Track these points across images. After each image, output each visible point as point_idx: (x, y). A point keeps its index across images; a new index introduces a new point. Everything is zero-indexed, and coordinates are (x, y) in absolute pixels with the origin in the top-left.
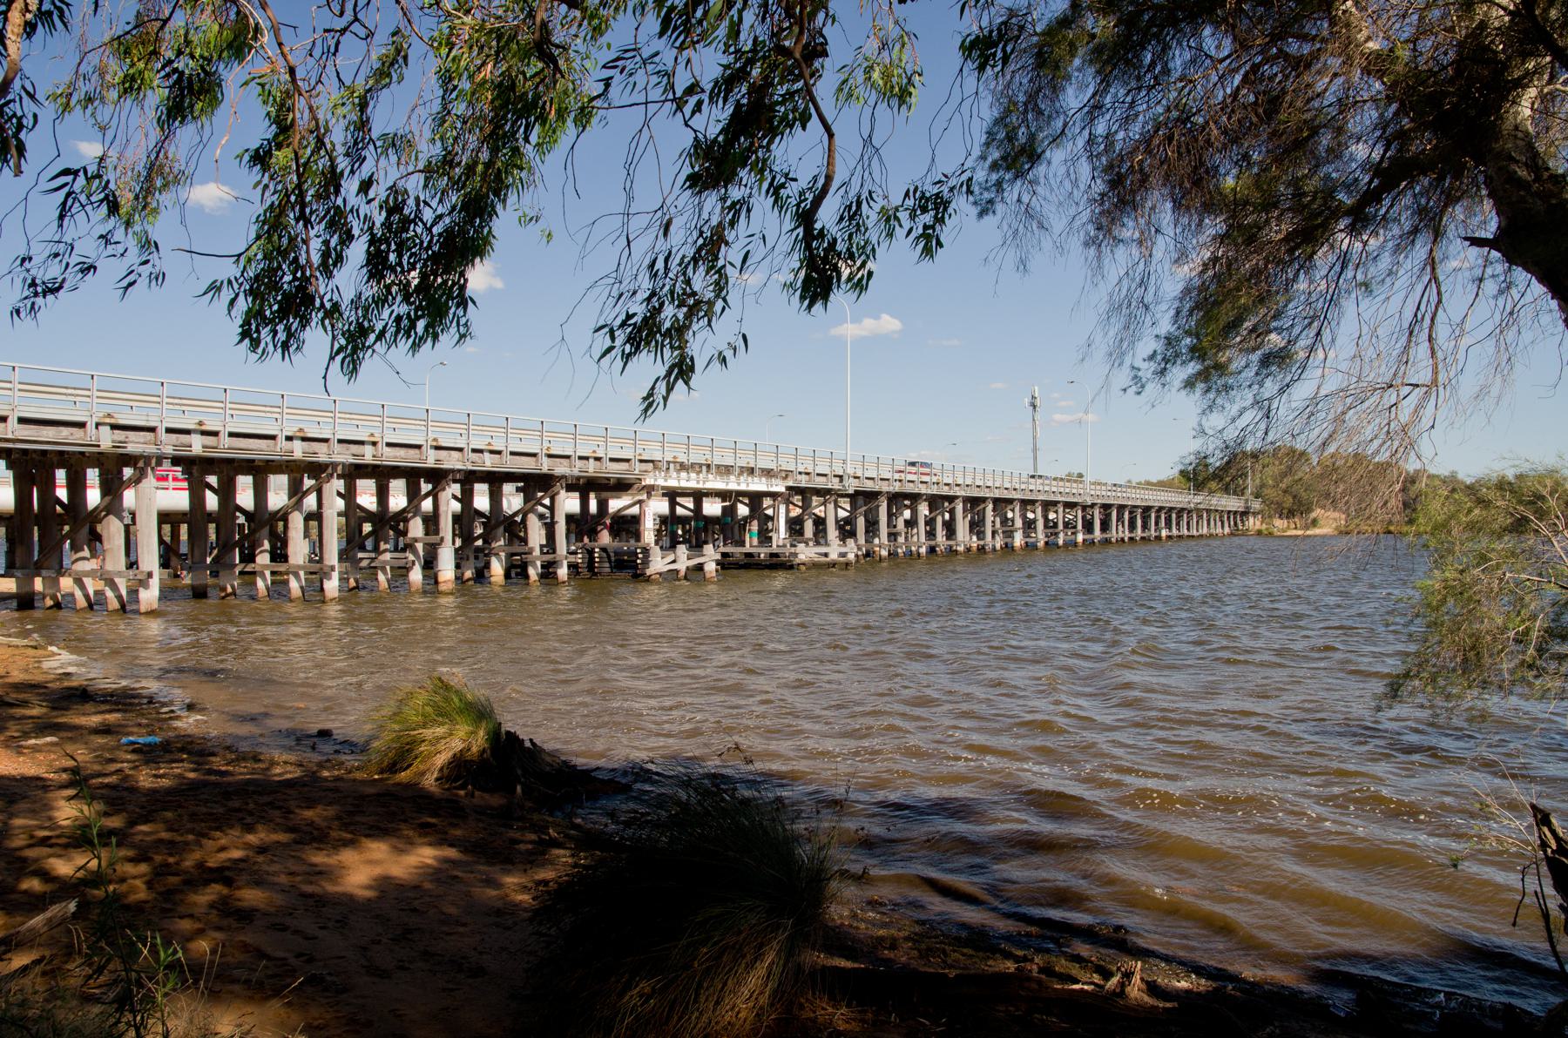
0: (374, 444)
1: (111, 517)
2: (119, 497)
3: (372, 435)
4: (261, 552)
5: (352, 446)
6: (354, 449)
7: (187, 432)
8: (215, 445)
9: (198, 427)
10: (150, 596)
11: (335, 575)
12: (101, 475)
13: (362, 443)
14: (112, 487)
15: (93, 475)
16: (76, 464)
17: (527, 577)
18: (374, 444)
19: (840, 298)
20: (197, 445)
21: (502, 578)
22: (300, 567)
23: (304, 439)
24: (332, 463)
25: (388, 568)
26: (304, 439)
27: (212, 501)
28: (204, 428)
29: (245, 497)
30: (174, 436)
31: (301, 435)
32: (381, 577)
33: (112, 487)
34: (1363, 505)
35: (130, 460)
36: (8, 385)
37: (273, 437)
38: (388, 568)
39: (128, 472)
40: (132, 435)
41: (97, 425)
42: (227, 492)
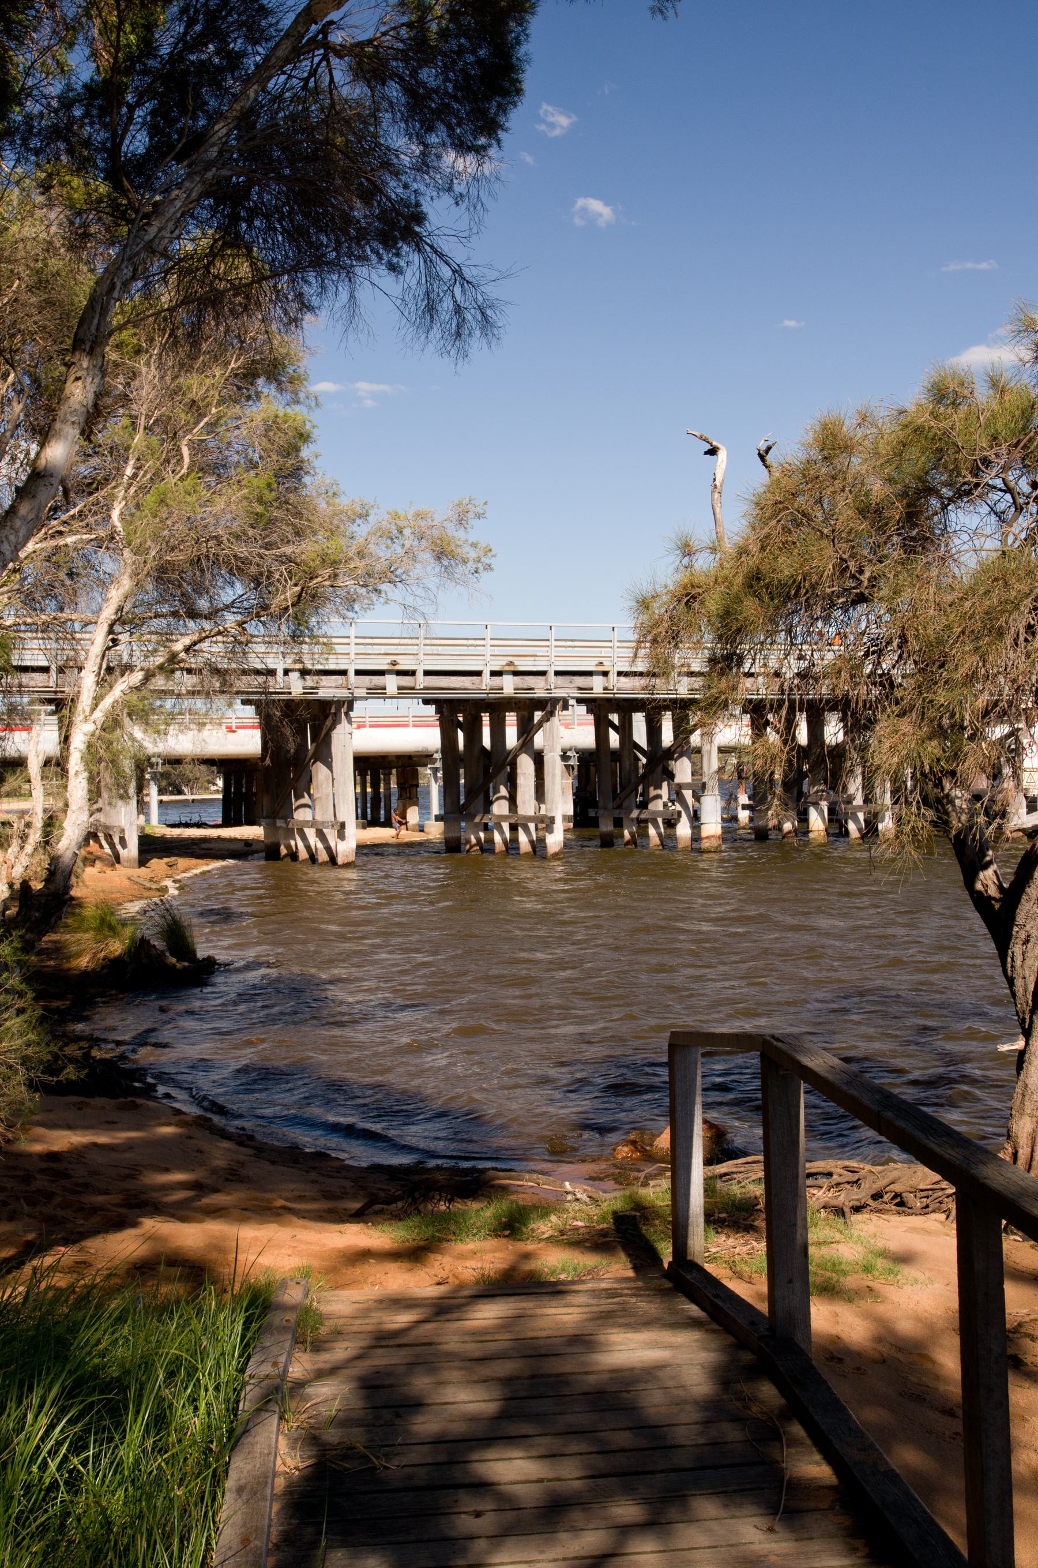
0: (605, 674)
1: (319, 764)
2: (687, 740)
3: (601, 664)
4: (498, 799)
5: (576, 678)
6: (580, 681)
7: (381, 673)
8: (411, 685)
9: (391, 667)
10: (555, 840)
11: (888, 815)
12: (646, 717)
13: (589, 674)
14: (526, 730)
15: (511, 719)
16: (497, 707)
17: (847, 833)
18: (605, 674)
19: (476, 344)
20: (597, 686)
21: (823, 833)
22: (530, 819)
23: (516, 673)
24: (551, 699)
25: (660, 820)
26: (516, 673)
27: (614, 739)
28: (397, 667)
29: (640, 735)
30: (367, 678)
31: (511, 668)
32: (652, 831)
33: (526, 730)
34: (150, 499)
35: (540, 704)
36: (414, 641)
37: (478, 673)
38: (660, 820)
39: (538, 715)
40: (326, 680)
41: (286, 672)
42: (625, 730)
